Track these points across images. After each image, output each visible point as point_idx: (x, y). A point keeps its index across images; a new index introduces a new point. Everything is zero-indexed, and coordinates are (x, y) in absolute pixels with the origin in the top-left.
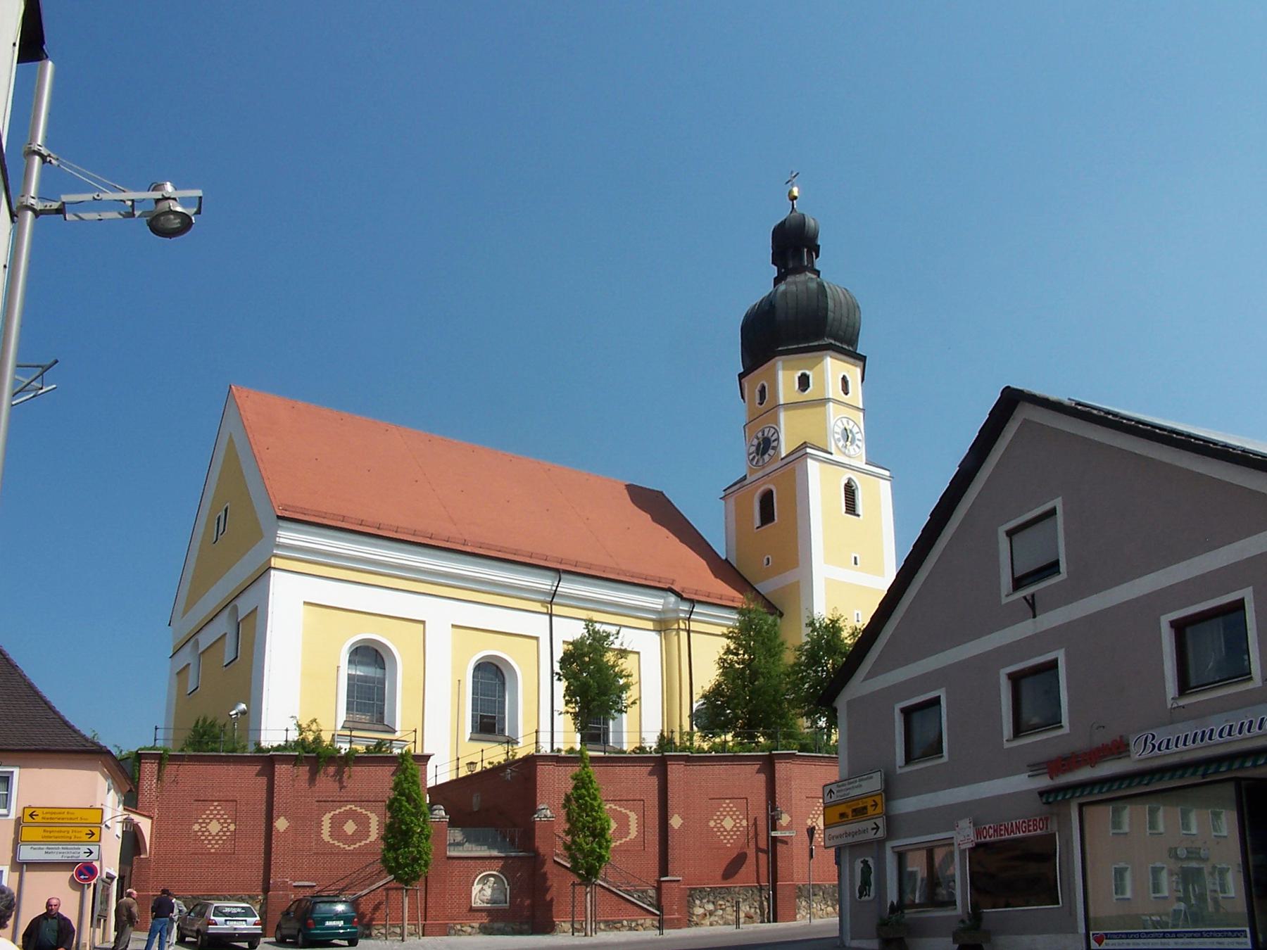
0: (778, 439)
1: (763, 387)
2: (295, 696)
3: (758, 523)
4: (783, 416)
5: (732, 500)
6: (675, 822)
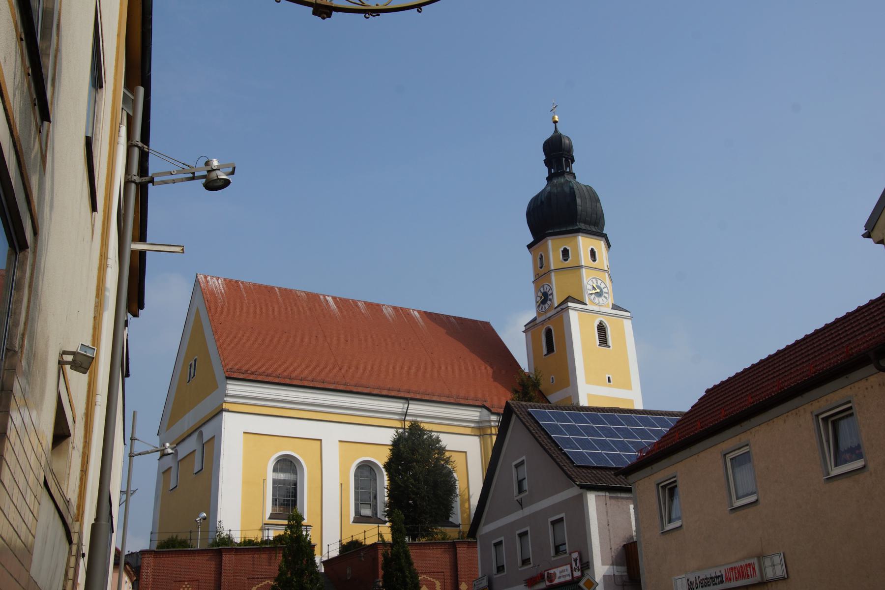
0: (551, 294)
2: (240, 510)
3: (545, 352)
5: (529, 333)
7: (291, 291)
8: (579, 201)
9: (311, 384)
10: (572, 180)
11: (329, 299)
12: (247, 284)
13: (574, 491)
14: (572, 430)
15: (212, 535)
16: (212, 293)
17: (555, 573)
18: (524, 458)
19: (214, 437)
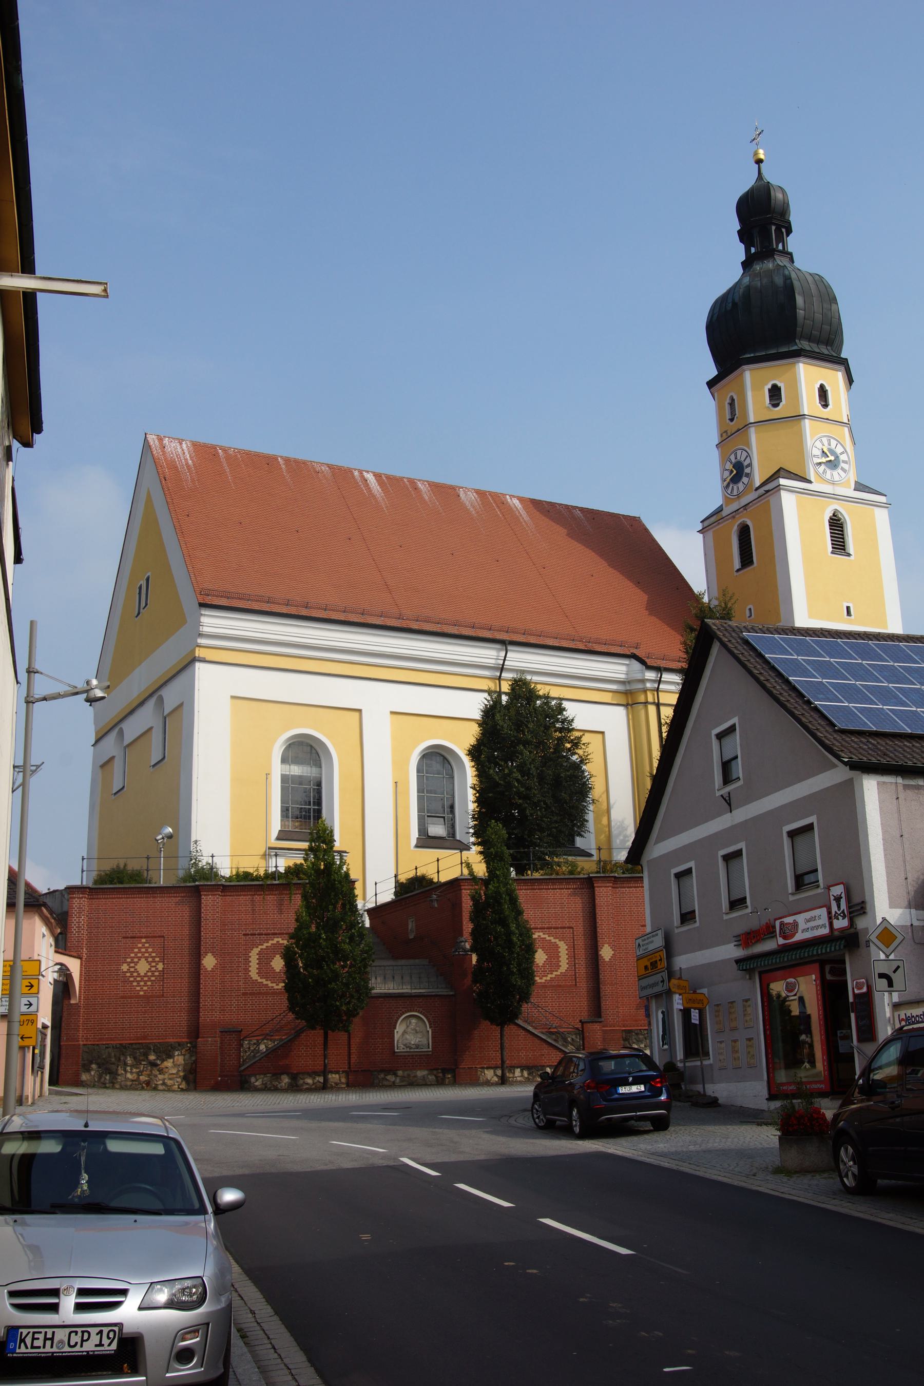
0: (750, 465)
1: (733, 400)
3: (737, 564)
4: (753, 435)
5: (710, 534)
6: (606, 953)
7: (305, 463)
8: (799, 300)
9: (342, 617)
10: (788, 265)
11: (370, 477)
12: (231, 452)
13: (838, 774)
14: (826, 670)
15: (183, 863)
16: (172, 466)
17: (795, 924)
18: (735, 720)
19: (181, 705)
